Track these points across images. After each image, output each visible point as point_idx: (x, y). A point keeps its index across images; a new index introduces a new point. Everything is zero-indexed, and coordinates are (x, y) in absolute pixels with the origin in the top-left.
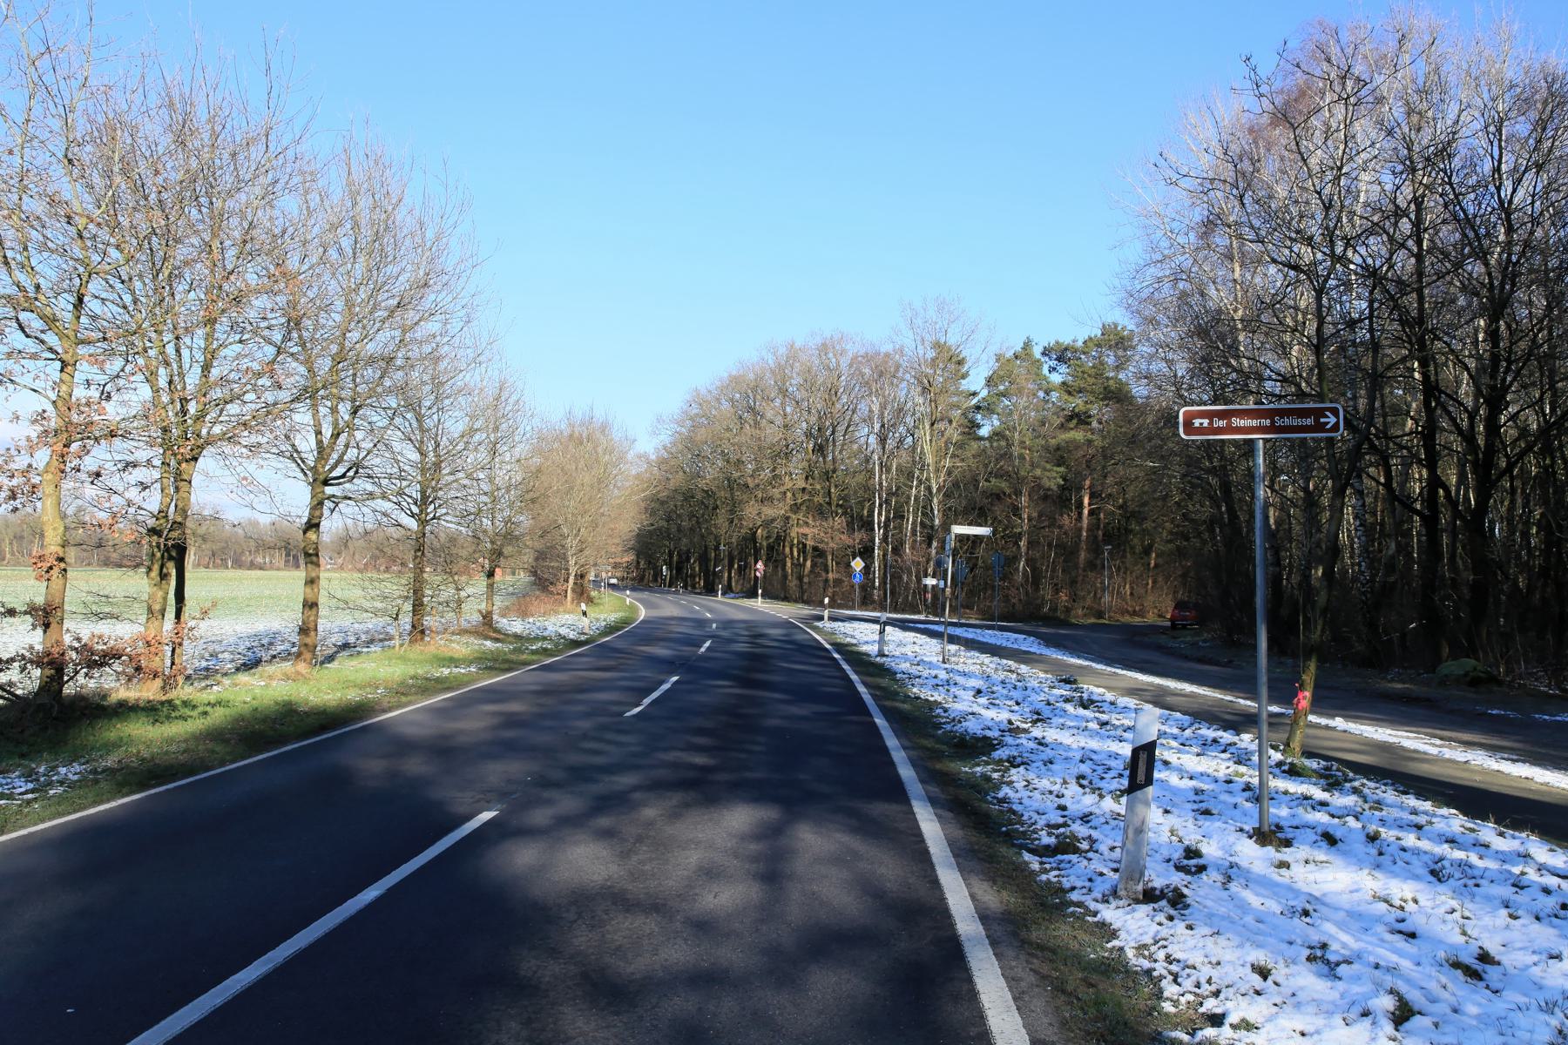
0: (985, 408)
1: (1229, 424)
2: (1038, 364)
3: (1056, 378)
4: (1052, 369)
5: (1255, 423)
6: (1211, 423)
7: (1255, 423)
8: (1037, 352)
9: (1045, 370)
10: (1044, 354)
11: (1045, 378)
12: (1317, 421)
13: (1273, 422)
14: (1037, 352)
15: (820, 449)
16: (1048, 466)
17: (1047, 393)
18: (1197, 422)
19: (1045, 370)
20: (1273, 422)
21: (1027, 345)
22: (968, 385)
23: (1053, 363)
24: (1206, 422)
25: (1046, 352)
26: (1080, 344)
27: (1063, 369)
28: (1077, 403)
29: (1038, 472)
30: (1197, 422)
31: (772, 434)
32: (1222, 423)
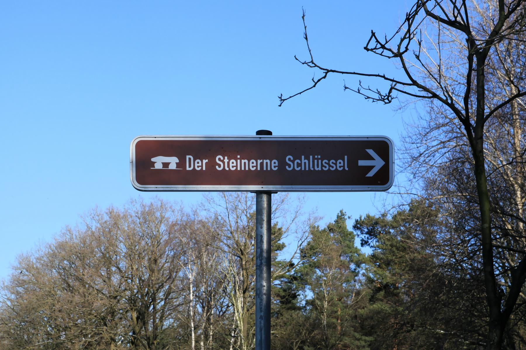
0: (300, 279)
1: (212, 165)
2: (350, 237)
3: (367, 251)
4: (364, 243)
5: (253, 165)
6: (181, 164)
7: (253, 165)
8: (349, 225)
9: (357, 243)
10: (355, 227)
11: (357, 251)
12: (353, 163)
13: (282, 164)
14: (349, 225)
15: (142, 317)
16: (357, 335)
17: (358, 265)
18: (159, 162)
19: (357, 243)
20: (282, 164)
21: (341, 217)
22: (283, 256)
23: (365, 236)
24: (173, 162)
25: (358, 226)
26: (389, 218)
27: (373, 242)
28: (388, 276)
29: (347, 340)
30: (159, 162)
31: (100, 304)
32: (200, 165)
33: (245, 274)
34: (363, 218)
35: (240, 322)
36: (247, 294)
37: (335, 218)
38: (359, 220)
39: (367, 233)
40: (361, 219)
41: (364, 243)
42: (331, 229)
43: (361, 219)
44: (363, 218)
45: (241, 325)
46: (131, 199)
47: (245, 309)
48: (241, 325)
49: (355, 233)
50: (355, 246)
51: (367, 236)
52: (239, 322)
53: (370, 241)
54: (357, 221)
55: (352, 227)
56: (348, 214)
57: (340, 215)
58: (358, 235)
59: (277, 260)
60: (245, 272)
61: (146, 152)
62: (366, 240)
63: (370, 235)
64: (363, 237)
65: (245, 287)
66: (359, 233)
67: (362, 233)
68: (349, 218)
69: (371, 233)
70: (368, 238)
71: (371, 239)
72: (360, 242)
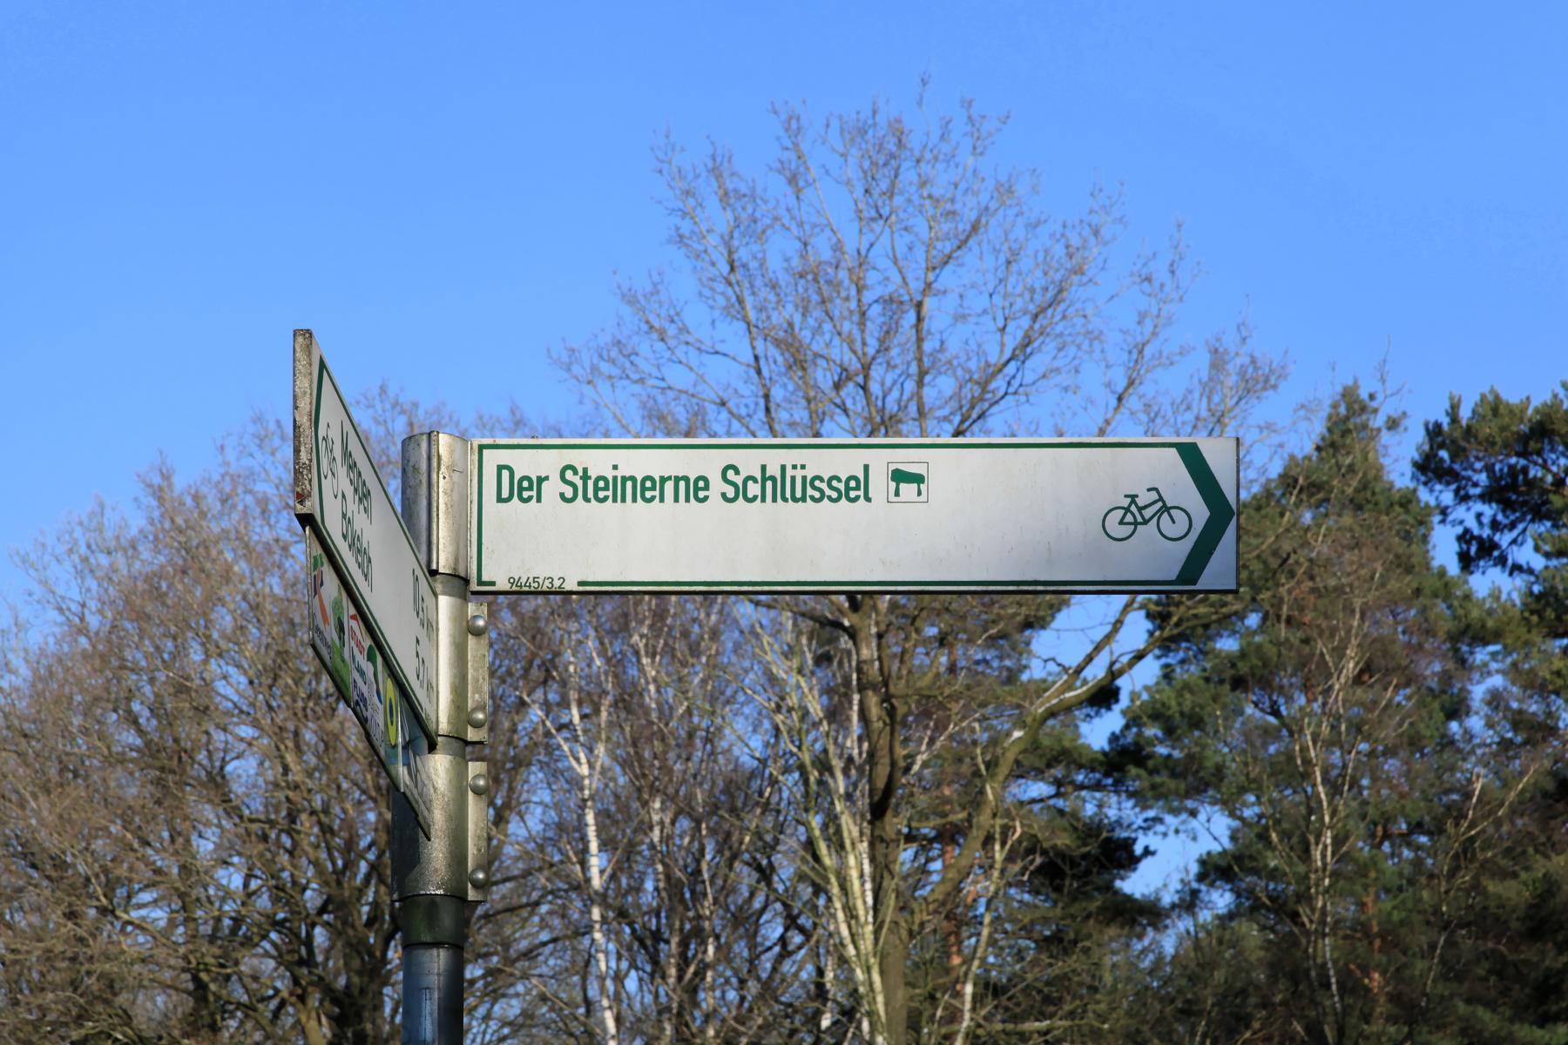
4: (1477, 551)
8: (1397, 460)
9: (1443, 550)
10: (1428, 468)
21: (1348, 426)
23: (1474, 515)
33: (875, 711)
34: (1465, 414)
35: (868, 970)
36: (896, 823)
37: (1317, 428)
38: (1445, 421)
39: (1486, 497)
40: (1454, 419)
41: (1477, 551)
42: (1299, 484)
43: (1454, 419)
44: (1465, 414)
45: (871, 980)
46: (258, 419)
47: (891, 901)
48: (871, 980)
49: (1424, 495)
50: (1435, 564)
51: (1489, 510)
52: (860, 974)
53: (1504, 539)
54: (1434, 432)
55: (1408, 469)
56: (1387, 409)
57: (1342, 410)
58: (1444, 512)
59: (1025, 677)
60: (873, 700)
61: (308, 334)
62: (1486, 532)
63: (1507, 505)
64: (1471, 523)
65: (881, 784)
66: (1447, 497)
67: (1462, 498)
68: (1410, 391)
69: (1515, 497)
70: (1495, 526)
71: (1512, 526)
72: (1455, 547)
